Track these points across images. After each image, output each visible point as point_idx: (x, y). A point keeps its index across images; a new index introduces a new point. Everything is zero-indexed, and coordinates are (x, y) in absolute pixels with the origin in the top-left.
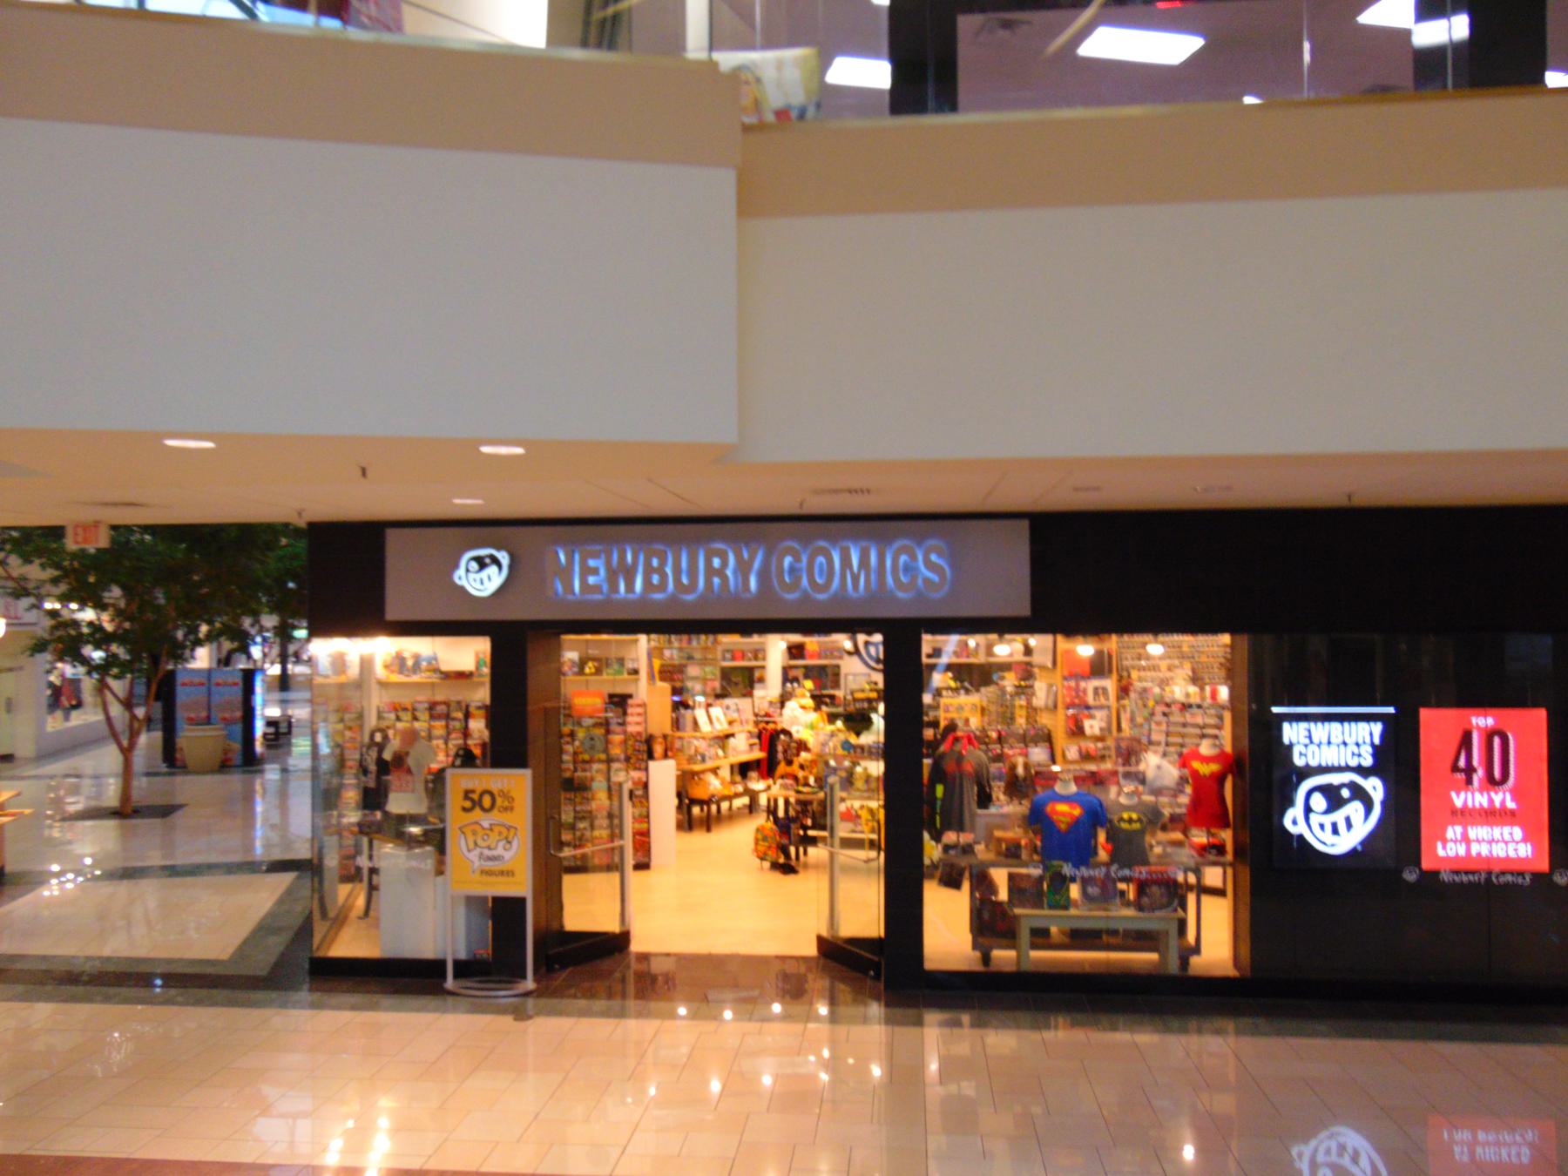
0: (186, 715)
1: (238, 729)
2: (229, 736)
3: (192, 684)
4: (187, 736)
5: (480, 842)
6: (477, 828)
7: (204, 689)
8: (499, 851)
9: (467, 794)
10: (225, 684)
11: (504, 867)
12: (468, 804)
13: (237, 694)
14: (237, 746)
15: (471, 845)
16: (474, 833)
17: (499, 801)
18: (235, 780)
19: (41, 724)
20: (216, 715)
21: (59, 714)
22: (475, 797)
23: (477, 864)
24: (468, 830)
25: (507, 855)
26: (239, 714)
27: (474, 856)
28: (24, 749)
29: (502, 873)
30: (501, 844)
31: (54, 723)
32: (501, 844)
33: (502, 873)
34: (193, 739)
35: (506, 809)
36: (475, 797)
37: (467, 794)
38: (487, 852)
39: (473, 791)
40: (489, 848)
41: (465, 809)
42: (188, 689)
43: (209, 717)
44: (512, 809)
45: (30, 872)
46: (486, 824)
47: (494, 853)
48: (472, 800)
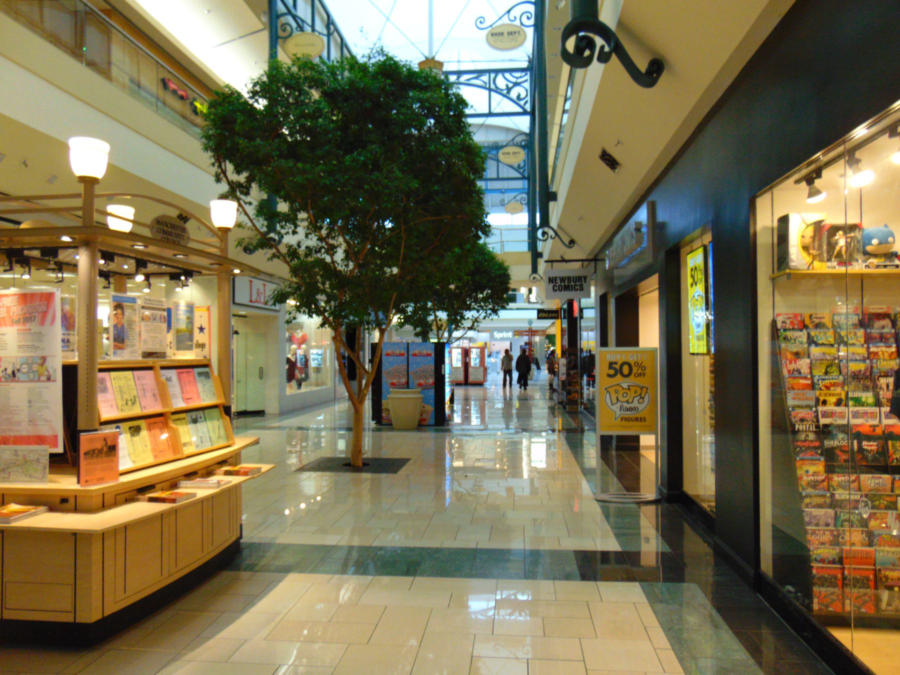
0: (390, 381)
1: (431, 393)
2: (424, 400)
3: (394, 355)
4: (393, 399)
5: (620, 398)
6: (619, 388)
7: (403, 359)
8: (635, 404)
9: (611, 365)
10: (421, 355)
11: (639, 416)
12: (612, 372)
13: (430, 363)
14: (431, 408)
15: (614, 401)
16: (616, 392)
17: (635, 369)
18: (428, 437)
19: (282, 390)
20: (414, 381)
21: (294, 383)
22: (617, 366)
23: (618, 413)
24: (612, 390)
25: (641, 407)
26: (431, 381)
27: (616, 408)
28: (272, 407)
29: (637, 419)
30: (636, 399)
31: (291, 390)
32: (636, 399)
33: (637, 419)
34: (397, 400)
35: (640, 375)
36: (617, 366)
37: (611, 365)
38: (625, 405)
39: (616, 363)
40: (627, 402)
41: (609, 376)
42: (390, 359)
43: (408, 383)
44: (644, 374)
45: (269, 545)
46: (625, 386)
47: (632, 405)
48: (615, 369)
